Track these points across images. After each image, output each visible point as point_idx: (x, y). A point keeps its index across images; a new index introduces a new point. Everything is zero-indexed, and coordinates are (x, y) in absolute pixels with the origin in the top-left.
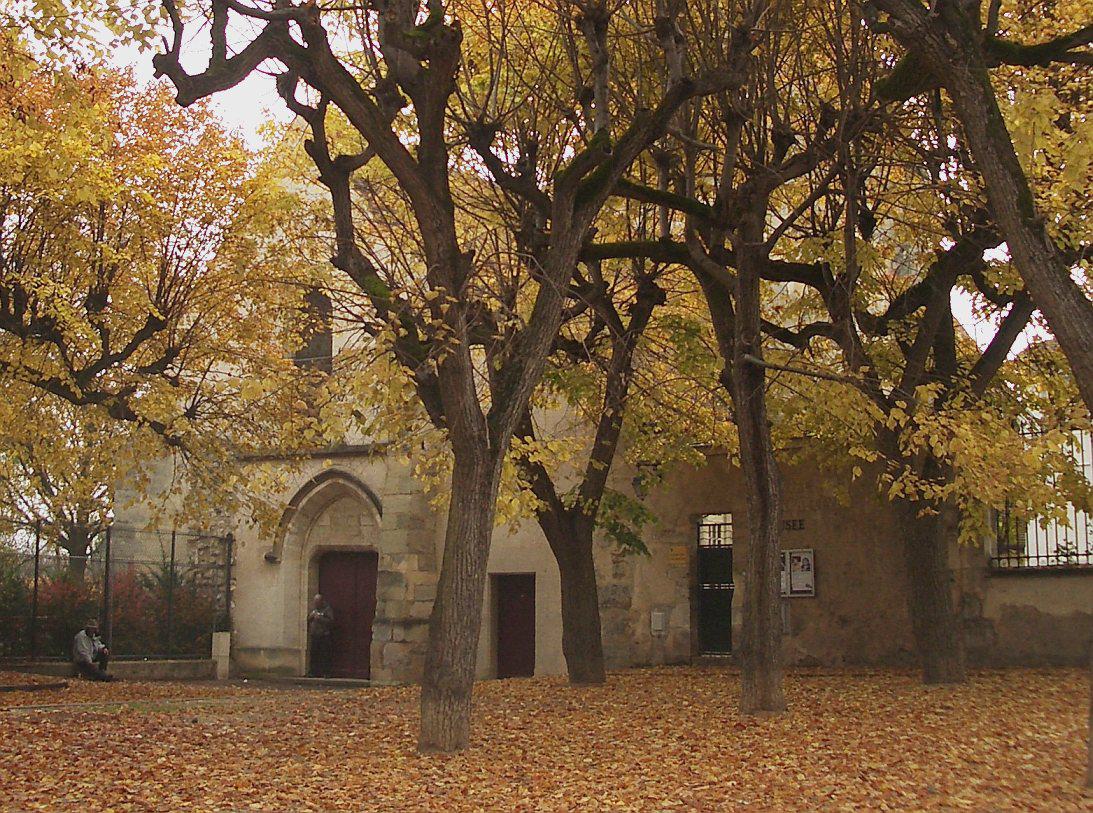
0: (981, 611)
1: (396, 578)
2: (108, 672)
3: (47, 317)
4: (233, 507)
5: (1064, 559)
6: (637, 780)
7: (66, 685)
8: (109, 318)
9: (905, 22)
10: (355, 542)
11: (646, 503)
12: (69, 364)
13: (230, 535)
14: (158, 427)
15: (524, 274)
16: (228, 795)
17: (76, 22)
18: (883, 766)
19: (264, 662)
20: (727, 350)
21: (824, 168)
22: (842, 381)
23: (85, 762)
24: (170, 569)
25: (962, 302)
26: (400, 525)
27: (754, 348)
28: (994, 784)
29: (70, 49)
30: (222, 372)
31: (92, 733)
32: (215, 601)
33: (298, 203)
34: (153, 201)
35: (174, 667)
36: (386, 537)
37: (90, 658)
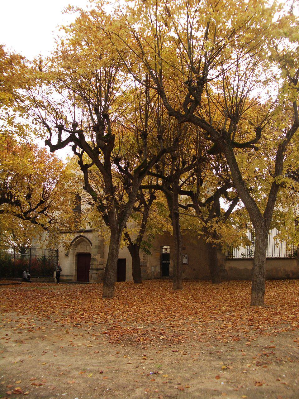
0: (224, 268)
1: (95, 259)
2: (30, 280)
3: (17, 200)
4: (59, 243)
5: (242, 257)
6: (152, 304)
7: (21, 283)
8: (31, 201)
9: (215, 137)
10: (86, 251)
11: (151, 243)
12: (22, 211)
13: (58, 250)
14: (42, 225)
15: (125, 192)
16: (61, 307)
17: (27, 133)
18: (206, 301)
19: (65, 278)
20: (171, 210)
21: (192, 171)
22: (196, 217)
23: (28, 300)
24: (44, 257)
25: (222, 200)
26: (96, 248)
27: (177, 209)
28: (231, 305)
29: (25, 139)
30: (57, 213)
31: (29, 294)
32: (54, 264)
33: (74, 175)
34: (42, 174)
35: (45, 279)
36: (92, 250)
37: (26, 277)
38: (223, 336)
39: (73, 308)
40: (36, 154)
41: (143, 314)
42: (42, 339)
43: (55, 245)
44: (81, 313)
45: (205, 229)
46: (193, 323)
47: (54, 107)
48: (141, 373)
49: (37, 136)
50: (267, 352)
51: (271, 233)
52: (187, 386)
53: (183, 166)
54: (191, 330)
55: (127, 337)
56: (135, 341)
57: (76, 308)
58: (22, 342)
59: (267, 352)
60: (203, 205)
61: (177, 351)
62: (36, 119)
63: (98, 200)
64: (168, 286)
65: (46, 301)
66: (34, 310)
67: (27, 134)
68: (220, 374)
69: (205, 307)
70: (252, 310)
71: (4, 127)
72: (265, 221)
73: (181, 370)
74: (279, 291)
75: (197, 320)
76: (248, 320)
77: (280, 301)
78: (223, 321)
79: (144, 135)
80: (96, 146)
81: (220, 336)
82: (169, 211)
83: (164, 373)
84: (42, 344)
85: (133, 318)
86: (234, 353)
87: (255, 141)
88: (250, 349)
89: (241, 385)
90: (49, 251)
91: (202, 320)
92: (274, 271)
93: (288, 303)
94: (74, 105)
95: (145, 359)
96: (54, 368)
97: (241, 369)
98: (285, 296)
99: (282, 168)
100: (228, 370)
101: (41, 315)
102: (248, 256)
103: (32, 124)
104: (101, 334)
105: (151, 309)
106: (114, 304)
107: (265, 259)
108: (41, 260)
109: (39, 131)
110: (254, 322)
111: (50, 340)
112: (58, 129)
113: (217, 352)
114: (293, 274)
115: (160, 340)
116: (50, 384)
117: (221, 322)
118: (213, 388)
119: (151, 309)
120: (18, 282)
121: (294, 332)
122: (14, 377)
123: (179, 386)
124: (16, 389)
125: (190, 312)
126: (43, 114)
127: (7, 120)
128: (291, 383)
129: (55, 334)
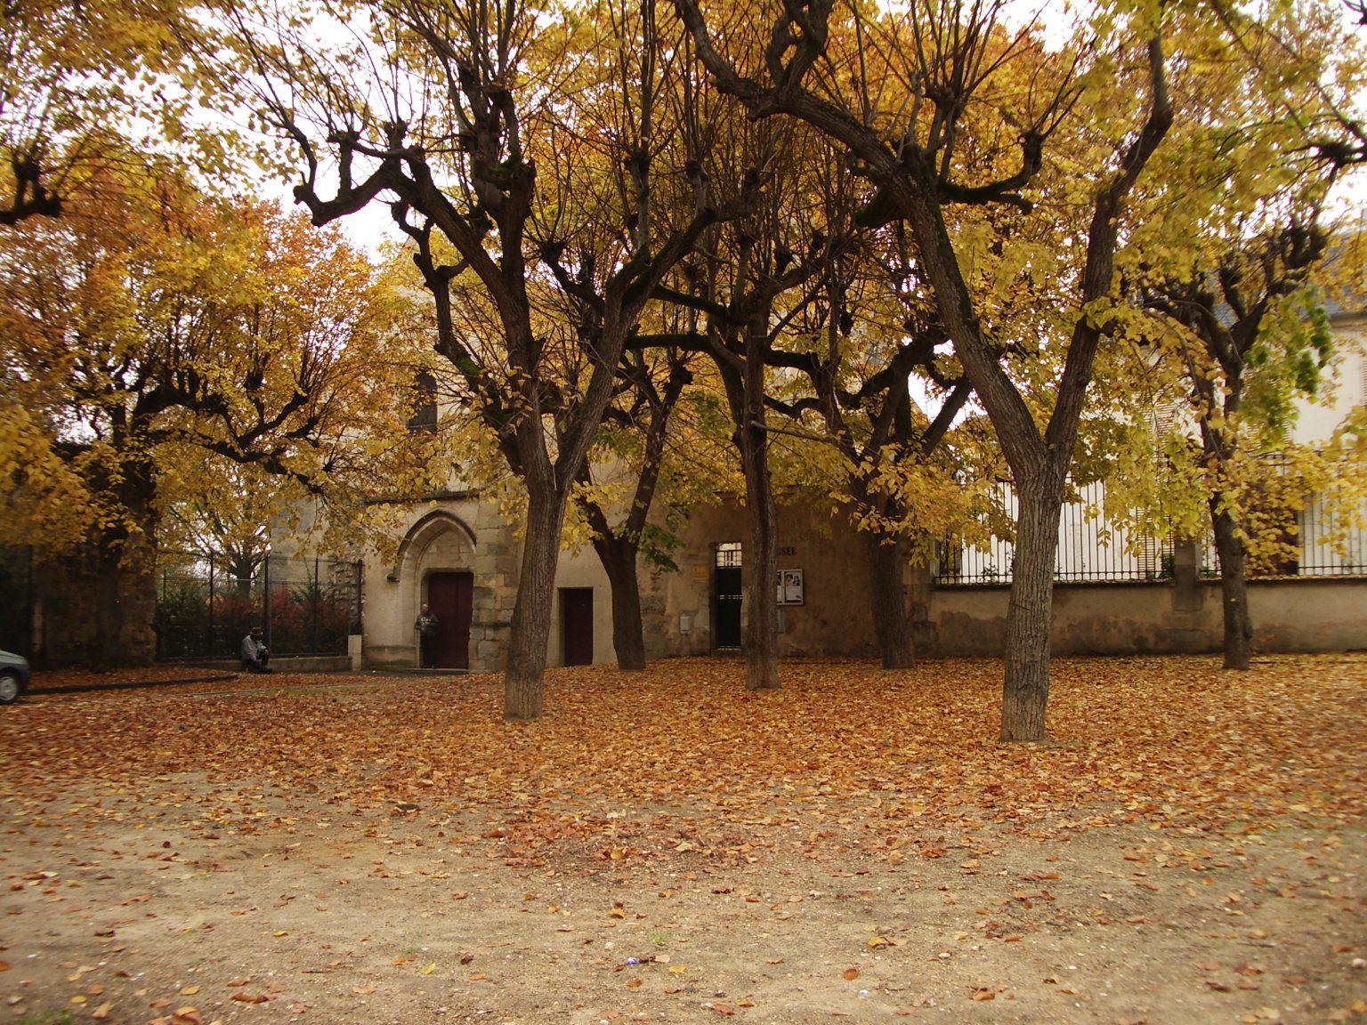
1: (487, 592)
2: (269, 666)
5: (988, 578)
6: (668, 739)
7: (236, 677)
9: (878, 167)
10: (455, 565)
11: (677, 534)
14: (303, 479)
15: (585, 359)
17: (231, 162)
18: (851, 728)
19: (388, 657)
20: (738, 418)
24: (314, 589)
26: (490, 552)
27: (759, 416)
28: (932, 740)
29: (228, 183)
31: (256, 711)
33: (410, 304)
37: (254, 657)
38: (889, 843)
39: (398, 755)
40: (273, 236)
41: (632, 770)
42: (283, 856)
43: (351, 544)
44: (423, 769)
45: (857, 486)
46: (795, 800)
47: (324, 71)
48: (599, 960)
49: (269, 174)
50: (1030, 891)
51: (1085, 498)
52: (744, 1002)
53: (781, 267)
54: (788, 821)
55: (566, 847)
56: (592, 860)
57: (407, 754)
58: (215, 866)
59: (1030, 891)
60: (852, 401)
61: (727, 892)
62: (261, 115)
63: (481, 388)
64: (732, 679)
65: (310, 734)
66: (265, 763)
67: (235, 166)
68: (862, 963)
69: (844, 747)
70: (1004, 757)
71: (150, 144)
72: (1052, 456)
73: (733, 953)
74: (1103, 693)
75: (810, 789)
76: (982, 789)
77: (1101, 727)
78: (899, 791)
79: (639, 161)
80: (475, 203)
81: (880, 842)
82: (734, 425)
83: (673, 962)
84: (280, 874)
85: (598, 786)
86: (919, 898)
87: (1019, 181)
88: (974, 883)
89: (923, 997)
90: (331, 567)
91: (829, 789)
92: (1096, 627)
93: (1126, 734)
94: (393, 62)
95: (620, 917)
96: (311, 946)
97: (934, 946)
98: (1121, 712)
99: (1110, 271)
100: (891, 949)
101: (288, 778)
102: (1006, 575)
103: (248, 132)
104: (483, 837)
105: (661, 754)
106: (538, 738)
107: (1050, 586)
108: (304, 598)
109: (273, 156)
110: (1002, 794)
111: (309, 859)
112: (337, 146)
113: (863, 893)
114: (1160, 635)
115: (677, 857)
116: (292, 996)
117: (892, 795)
118: (830, 1009)
119: (661, 754)
120: (225, 673)
121: (1132, 828)
122: (177, 974)
123: (718, 1000)
124: (181, 1012)
125: (792, 762)
126: (284, 94)
127: (158, 119)
128: (1092, 990)
129: (328, 839)
